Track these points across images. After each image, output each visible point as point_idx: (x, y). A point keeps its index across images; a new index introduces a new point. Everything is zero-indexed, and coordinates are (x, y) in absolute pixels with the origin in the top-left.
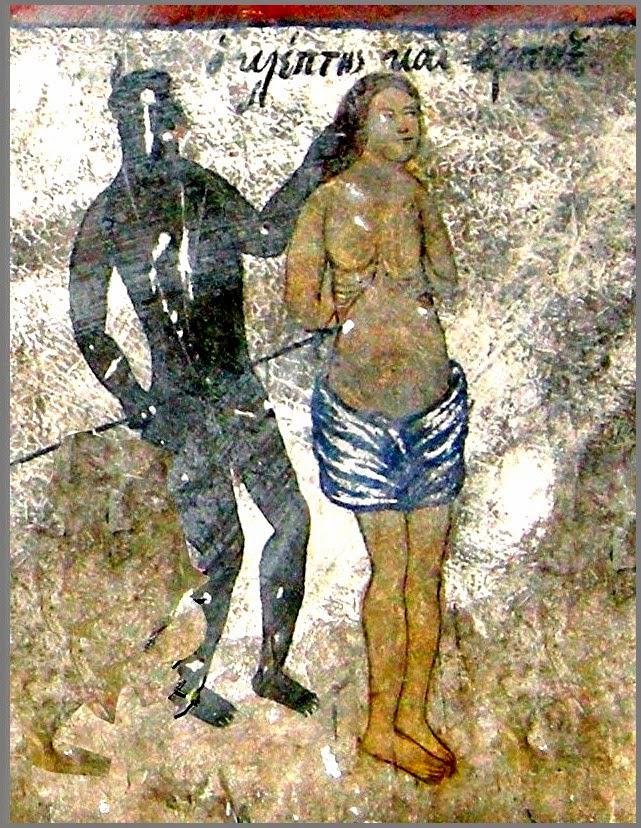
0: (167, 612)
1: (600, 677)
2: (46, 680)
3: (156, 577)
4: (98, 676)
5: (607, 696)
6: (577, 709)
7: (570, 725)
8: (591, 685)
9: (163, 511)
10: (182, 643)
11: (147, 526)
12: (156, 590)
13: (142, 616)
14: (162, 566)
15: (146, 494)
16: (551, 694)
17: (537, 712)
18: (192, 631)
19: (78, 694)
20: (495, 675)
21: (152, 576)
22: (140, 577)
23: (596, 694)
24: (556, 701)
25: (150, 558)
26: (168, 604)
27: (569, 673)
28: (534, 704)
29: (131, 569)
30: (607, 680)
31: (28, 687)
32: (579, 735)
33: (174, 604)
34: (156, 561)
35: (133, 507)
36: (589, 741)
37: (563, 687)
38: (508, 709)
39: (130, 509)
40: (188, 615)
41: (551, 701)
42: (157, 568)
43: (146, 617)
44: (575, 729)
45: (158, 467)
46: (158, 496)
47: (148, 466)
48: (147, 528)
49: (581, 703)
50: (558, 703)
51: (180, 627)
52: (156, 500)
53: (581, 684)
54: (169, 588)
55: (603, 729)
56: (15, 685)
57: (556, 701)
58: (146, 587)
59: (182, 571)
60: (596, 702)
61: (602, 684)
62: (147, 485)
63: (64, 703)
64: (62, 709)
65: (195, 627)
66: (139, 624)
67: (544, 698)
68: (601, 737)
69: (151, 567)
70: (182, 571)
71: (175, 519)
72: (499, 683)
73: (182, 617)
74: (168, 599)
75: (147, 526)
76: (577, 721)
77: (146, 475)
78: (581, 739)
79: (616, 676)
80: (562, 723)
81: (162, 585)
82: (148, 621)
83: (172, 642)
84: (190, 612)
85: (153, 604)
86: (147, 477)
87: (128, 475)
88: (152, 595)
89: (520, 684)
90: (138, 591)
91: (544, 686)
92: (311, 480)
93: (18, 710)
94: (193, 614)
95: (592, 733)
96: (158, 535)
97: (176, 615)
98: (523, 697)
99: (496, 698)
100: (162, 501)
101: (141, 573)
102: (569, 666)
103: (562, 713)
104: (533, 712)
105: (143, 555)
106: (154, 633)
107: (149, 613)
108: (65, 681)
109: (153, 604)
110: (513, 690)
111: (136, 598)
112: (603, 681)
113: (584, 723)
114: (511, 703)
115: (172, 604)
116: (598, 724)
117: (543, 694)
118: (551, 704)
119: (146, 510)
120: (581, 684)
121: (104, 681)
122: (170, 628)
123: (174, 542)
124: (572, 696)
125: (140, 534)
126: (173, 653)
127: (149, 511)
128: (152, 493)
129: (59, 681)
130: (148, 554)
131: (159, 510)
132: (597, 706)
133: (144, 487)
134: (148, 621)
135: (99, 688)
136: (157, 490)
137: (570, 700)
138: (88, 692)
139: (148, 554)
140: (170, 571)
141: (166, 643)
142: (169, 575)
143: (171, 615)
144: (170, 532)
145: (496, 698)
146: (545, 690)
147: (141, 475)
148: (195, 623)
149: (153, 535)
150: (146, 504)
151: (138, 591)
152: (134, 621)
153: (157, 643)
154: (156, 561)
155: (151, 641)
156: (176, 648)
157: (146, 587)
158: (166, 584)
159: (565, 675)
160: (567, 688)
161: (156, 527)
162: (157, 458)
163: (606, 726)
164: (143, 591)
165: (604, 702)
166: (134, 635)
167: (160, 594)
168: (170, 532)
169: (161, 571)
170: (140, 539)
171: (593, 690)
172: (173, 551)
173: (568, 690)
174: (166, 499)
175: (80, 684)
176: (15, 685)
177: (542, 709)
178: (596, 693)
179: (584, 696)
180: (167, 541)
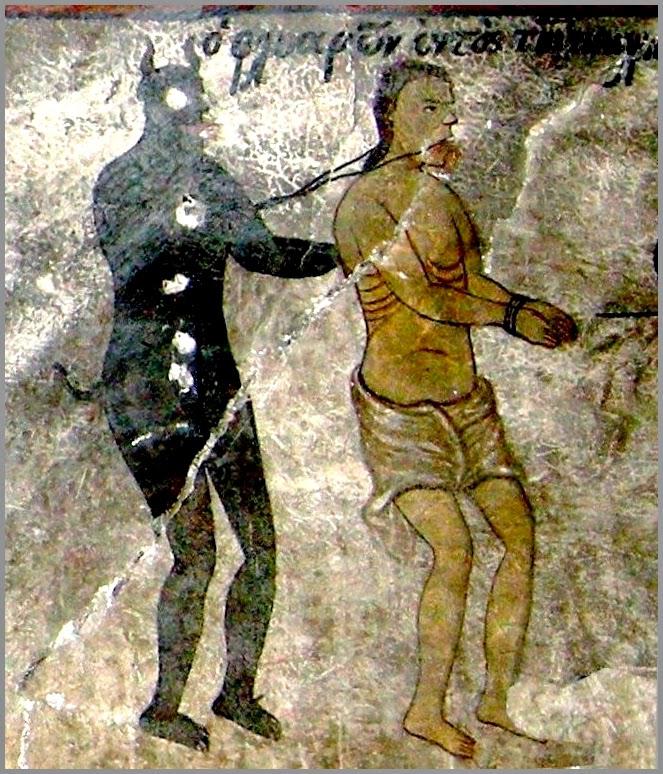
0: (47, 643)
1: (633, 696)
2: (554, 692)
3: (35, 608)
4: (607, 689)
5: (640, 715)
6: (610, 728)
7: (603, 745)
8: (624, 703)
9: (44, 542)
10: (61, 675)
11: (28, 557)
12: (36, 621)
13: (21, 647)
14: (43, 597)
15: (27, 525)
16: (584, 712)
17: (570, 731)
18: (71, 662)
19: (587, 707)
20: (528, 692)
21: (32, 607)
22: (20, 608)
23: (630, 713)
24: (589, 720)
25: (30, 590)
26: (47, 635)
27: (603, 690)
28: (567, 723)
29: (11, 600)
30: (641, 699)
31: (537, 699)
32: (612, 756)
33: (53, 635)
34: (36, 592)
35: (14, 539)
36: (622, 762)
37: (596, 705)
38: (541, 728)
39: (11, 539)
40: (67, 646)
41: (584, 720)
42: (37, 599)
43: (25, 648)
44: (608, 750)
45: (41, 498)
46: (39, 527)
47: (30, 497)
48: (27, 559)
49: (614, 723)
50: (592, 722)
51: (60, 659)
52: (37, 532)
53: (614, 702)
54: (48, 620)
55: (636, 749)
56: (524, 697)
57: (589, 720)
58: (27, 617)
59: (62, 603)
60: (629, 721)
61: (635, 703)
62: (28, 515)
63: (572, 716)
64: (571, 722)
65: (74, 659)
66: (19, 656)
67: (578, 716)
68: (633, 758)
69: (31, 598)
70: (62, 603)
71: (56, 551)
72: (533, 700)
73: (62, 649)
74: (48, 631)
75: (28, 557)
76: (610, 741)
77: (27, 506)
78: (613, 760)
79: (650, 694)
80: (595, 743)
81: (43, 616)
82: (27, 652)
83: (51, 673)
84: (69, 644)
85: (32, 635)
86: (29, 508)
87: (10, 506)
88: (31, 626)
89: (553, 701)
90: (18, 622)
91: (577, 704)
92: (217, 511)
93: (526, 723)
94: (72, 646)
95: (625, 754)
96: (39, 566)
97: (56, 647)
98: (556, 715)
99: (530, 716)
100: (44, 532)
101: (21, 604)
102: (602, 683)
103: (595, 733)
104: (567, 731)
105: (23, 586)
106: (33, 665)
107: (28, 644)
108: (573, 693)
109: (32, 635)
110: (547, 708)
111: (16, 629)
112: (636, 700)
113: (616, 743)
114: (544, 721)
115: (52, 635)
116: (631, 744)
117: (576, 713)
118: (584, 723)
119: (27, 542)
120: (614, 702)
121: (613, 694)
122: (49, 659)
123: (55, 573)
124: (605, 715)
125: (21, 565)
126: (52, 685)
127: (30, 542)
128: (33, 525)
129: (568, 693)
130: (28, 585)
131: (40, 541)
132: (630, 726)
133: (25, 517)
134: (27, 652)
135: (607, 702)
136: (38, 521)
137: (603, 719)
138: (596, 705)
139: (28, 585)
140: (50, 603)
141: (44, 674)
142: (48, 606)
143: (50, 646)
144: (51, 563)
145: (530, 716)
146: (578, 708)
147: (22, 506)
148: (75, 655)
149: (34, 566)
150: (28, 535)
151: (18, 622)
152: (14, 651)
153: (36, 674)
154: (36, 592)
155: (30, 672)
156: (55, 680)
157: (27, 617)
158: (45, 616)
159: (599, 693)
160: (600, 706)
161: (37, 559)
162: (38, 490)
163: (639, 747)
164: (22, 622)
165: (636, 722)
166: (13, 666)
167: (40, 625)
168: (51, 563)
169: (41, 603)
170: (21, 570)
171: (626, 709)
172: (53, 583)
173: (601, 708)
174: (48, 531)
175: (589, 697)
176: (524, 697)
177: (575, 728)
178: (629, 712)
179: (617, 715)
180: (48, 573)
